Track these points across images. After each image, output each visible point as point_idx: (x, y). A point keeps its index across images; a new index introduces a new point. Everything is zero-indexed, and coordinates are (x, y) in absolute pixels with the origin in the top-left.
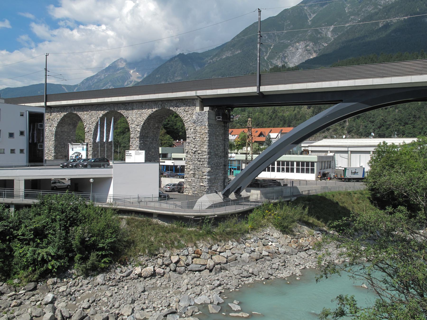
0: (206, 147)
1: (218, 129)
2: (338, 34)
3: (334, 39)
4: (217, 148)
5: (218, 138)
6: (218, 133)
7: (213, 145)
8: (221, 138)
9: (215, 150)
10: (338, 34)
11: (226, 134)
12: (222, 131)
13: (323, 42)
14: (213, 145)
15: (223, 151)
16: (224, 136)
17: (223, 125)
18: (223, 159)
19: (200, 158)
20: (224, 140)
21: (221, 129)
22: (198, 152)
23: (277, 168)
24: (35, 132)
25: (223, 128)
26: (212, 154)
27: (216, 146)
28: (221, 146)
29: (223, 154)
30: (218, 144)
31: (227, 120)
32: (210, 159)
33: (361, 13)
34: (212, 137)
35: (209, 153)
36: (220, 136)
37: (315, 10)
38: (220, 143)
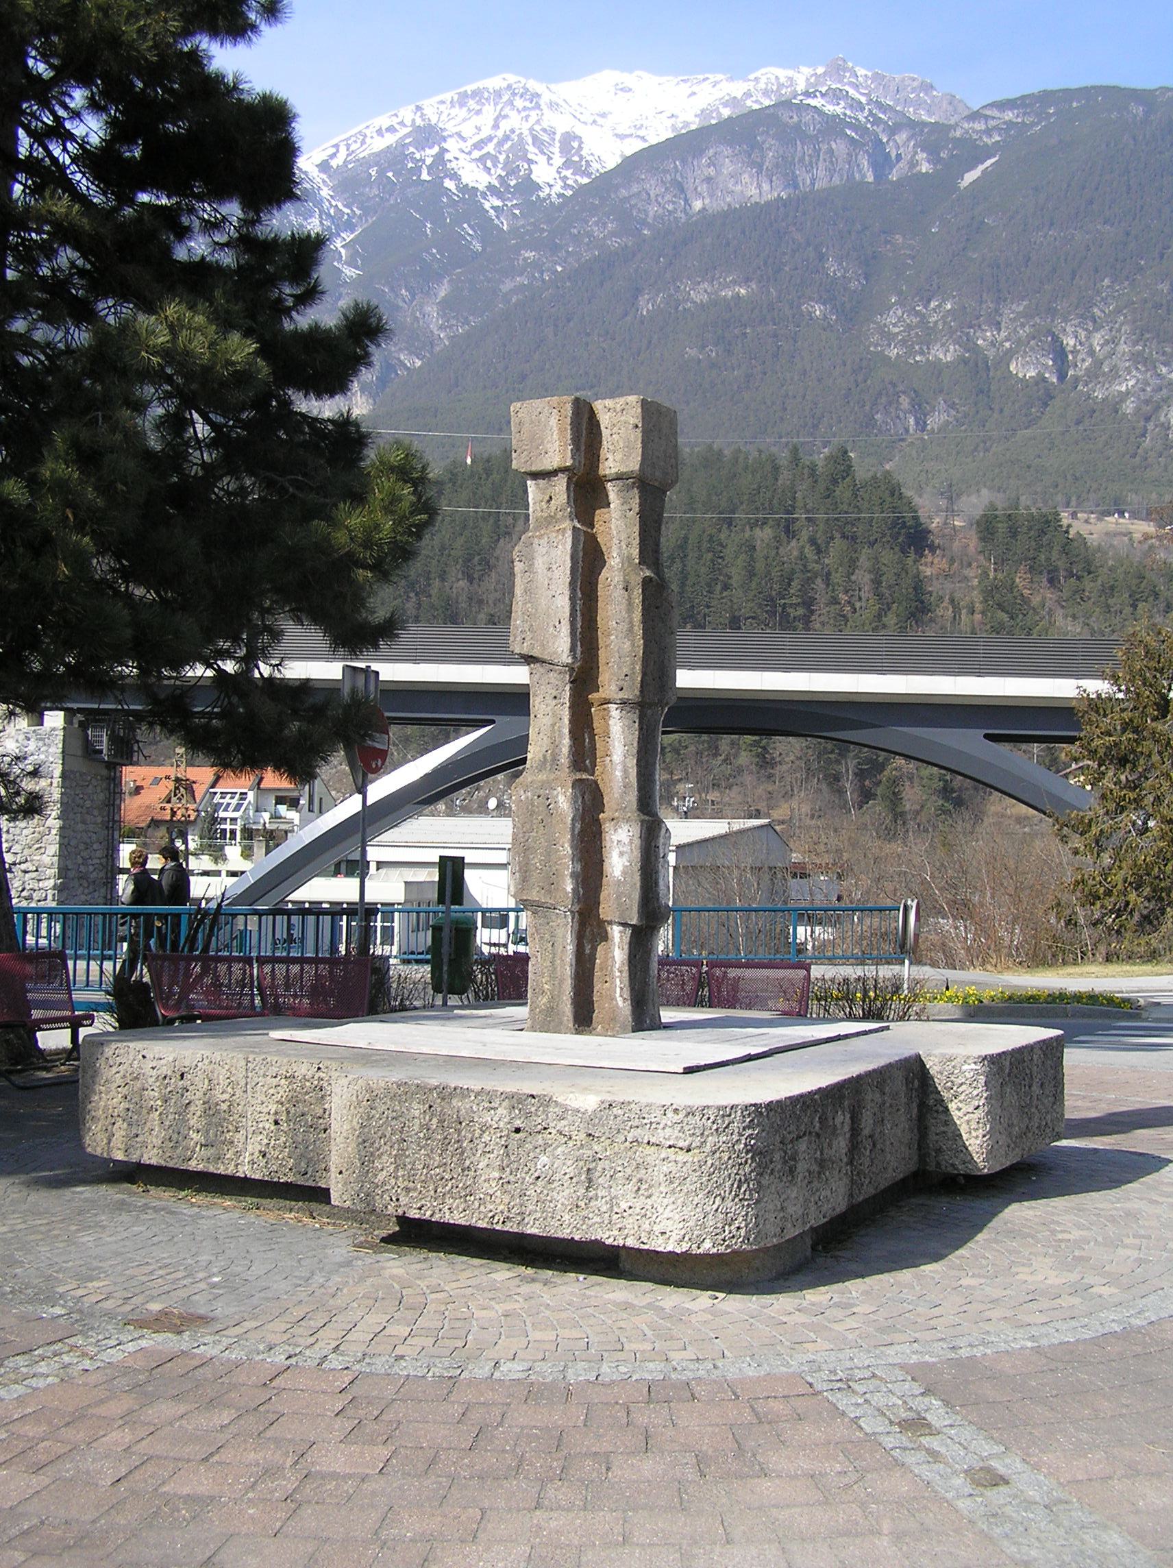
0: (53, 849)
1: (90, 790)
2: (467, 322)
3: (451, 338)
4: (85, 854)
5: (88, 818)
6: (88, 804)
7: (73, 843)
8: (99, 820)
9: (80, 861)
10: (467, 322)
11: (113, 805)
12: (102, 797)
13: (400, 349)
14: (73, 843)
15: (101, 864)
16: (105, 814)
17: (105, 772)
18: (103, 891)
19: (28, 887)
20: (107, 828)
21: (99, 789)
22: (23, 867)
23: (383, 928)
24: (1118, 1024)
25: (104, 785)
26: (71, 874)
27: (82, 847)
28: (95, 846)
29: (102, 874)
30: (88, 841)
31: (122, 757)
32: (65, 894)
33: (568, 245)
34: (71, 816)
35: (63, 872)
36: (96, 812)
37: (369, 199)
38: (94, 837)
